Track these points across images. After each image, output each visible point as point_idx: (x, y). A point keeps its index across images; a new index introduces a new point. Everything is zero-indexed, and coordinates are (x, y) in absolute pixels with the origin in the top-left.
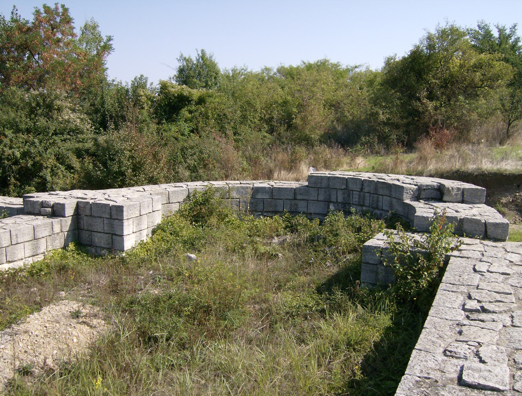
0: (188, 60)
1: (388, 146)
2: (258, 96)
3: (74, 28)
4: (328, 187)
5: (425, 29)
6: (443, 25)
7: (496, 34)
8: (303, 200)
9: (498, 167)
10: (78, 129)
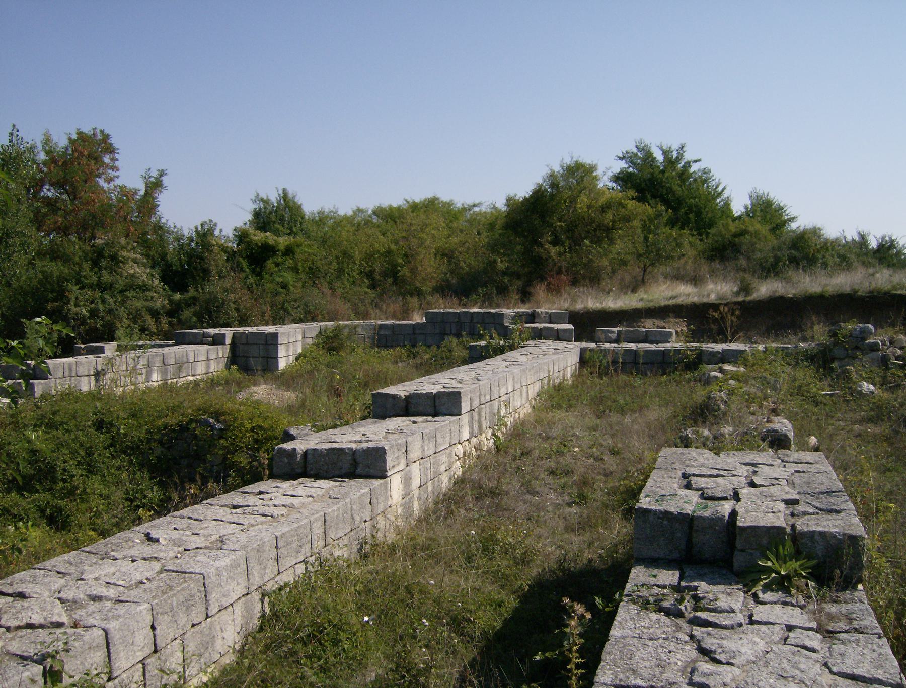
0: (266, 202)
2: (356, 245)
3: (117, 160)
5: (547, 166)
6: (568, 161)
7: (659, 157)
10: (145, 286)
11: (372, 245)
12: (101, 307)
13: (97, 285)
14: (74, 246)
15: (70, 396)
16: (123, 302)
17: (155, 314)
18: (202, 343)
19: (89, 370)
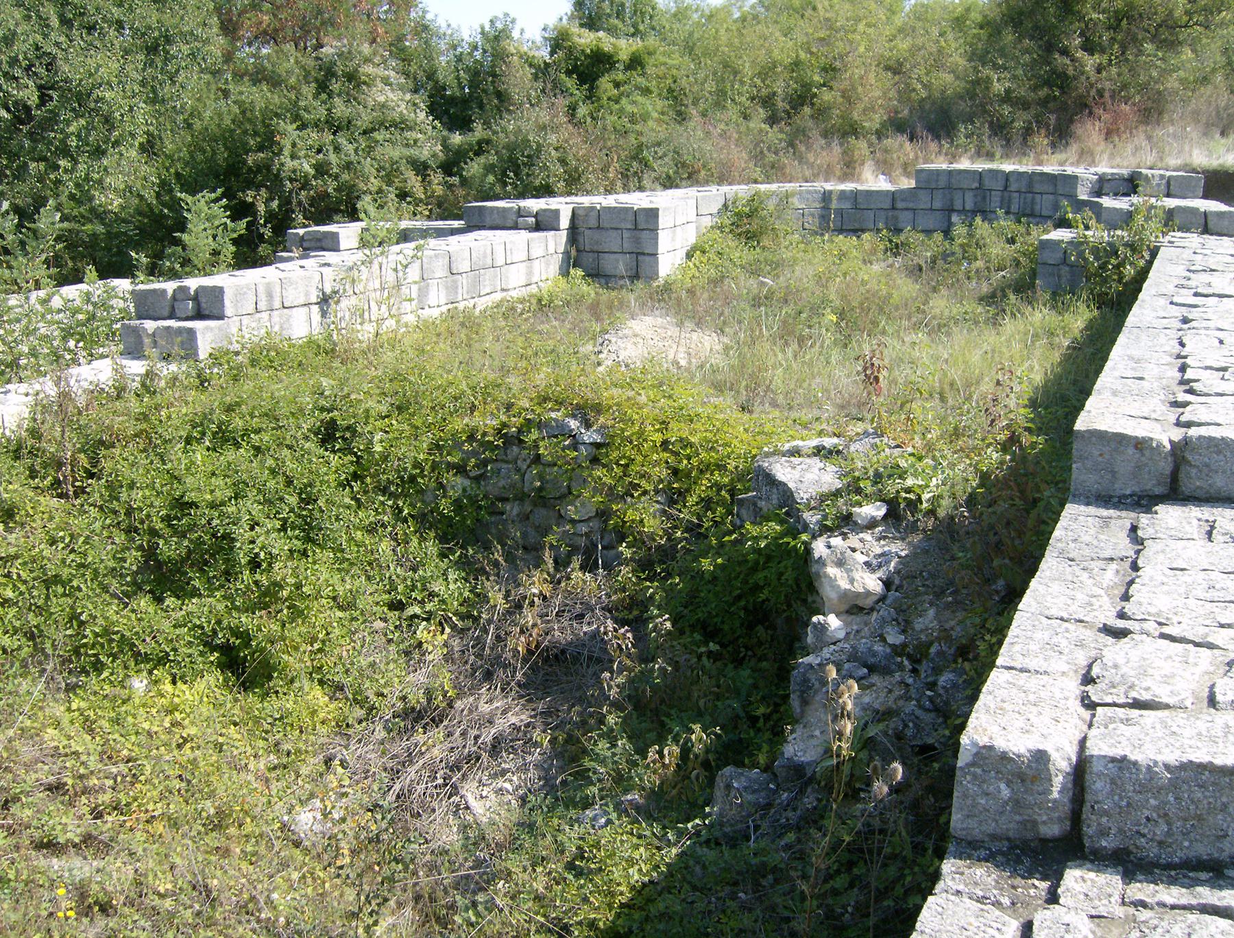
1: (1008, 141)
4: (949, 188)
8: (907, 209)
9: (1221, 161)
11: (769, 52)
12: (333, 158)
13: (327, 122)
14: (289, 61)
15: (268, 356)
16: (370, 149)
17: (421, 168)
18: (516, 227)
19: (307, 294)
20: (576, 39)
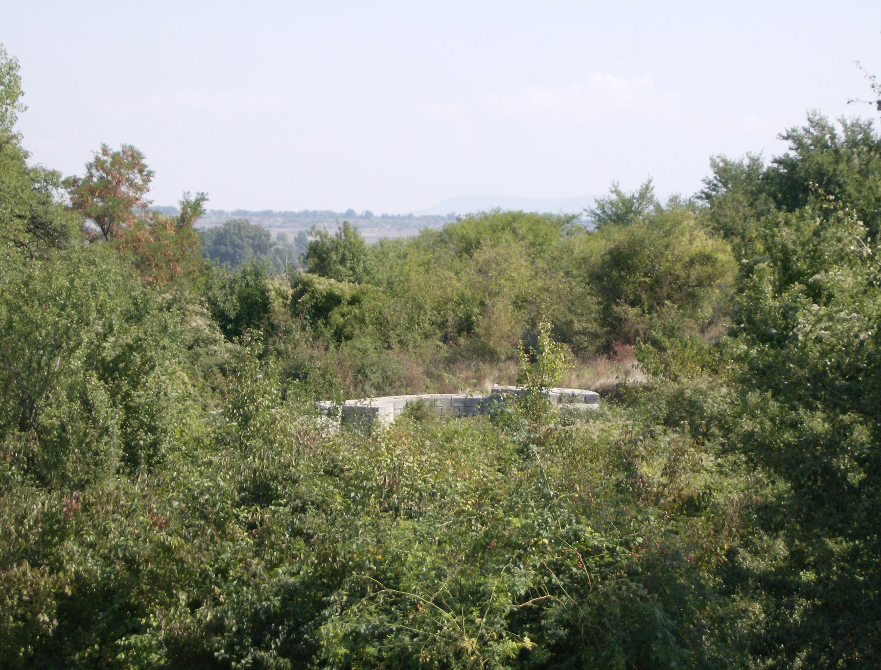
20: (317, 286)
